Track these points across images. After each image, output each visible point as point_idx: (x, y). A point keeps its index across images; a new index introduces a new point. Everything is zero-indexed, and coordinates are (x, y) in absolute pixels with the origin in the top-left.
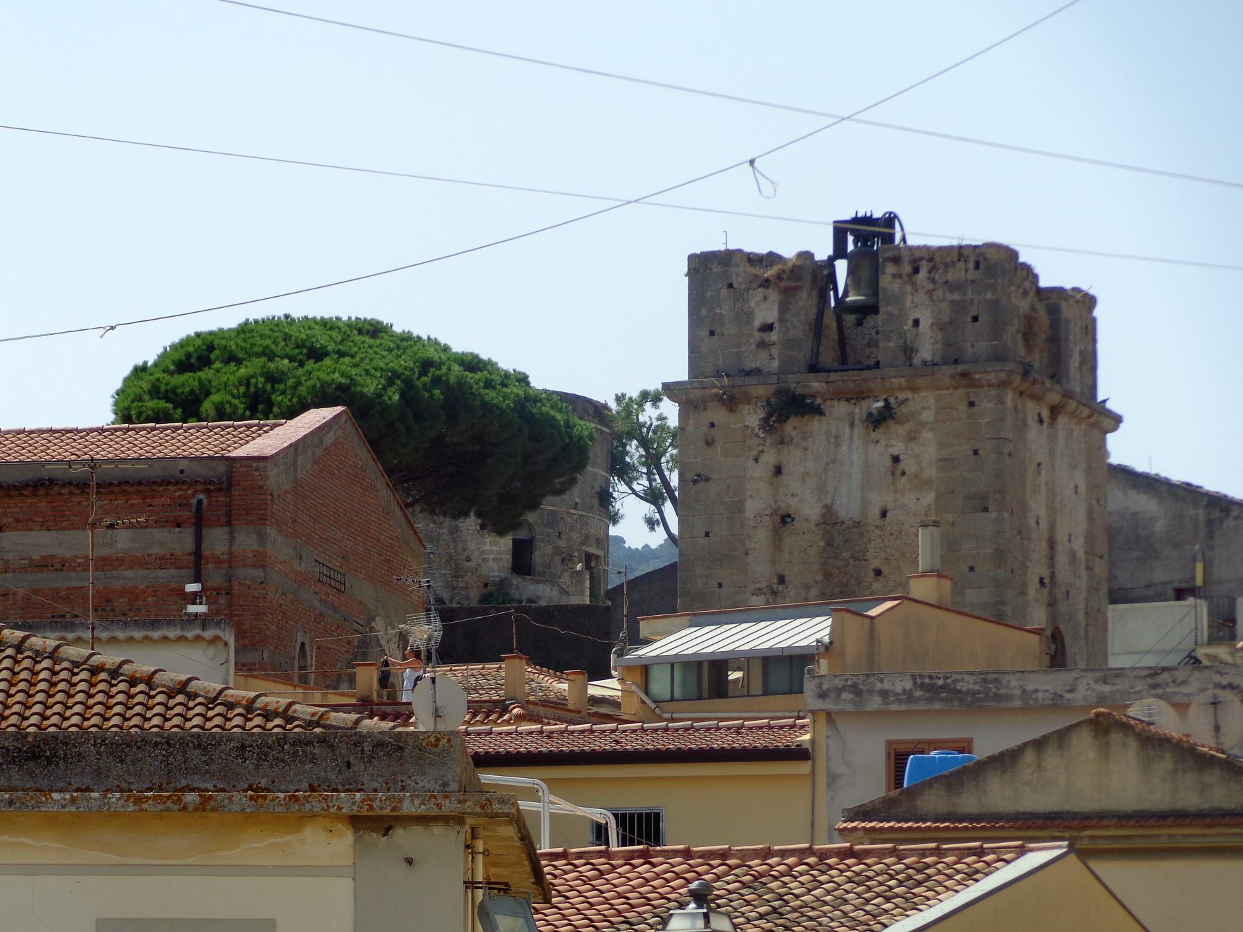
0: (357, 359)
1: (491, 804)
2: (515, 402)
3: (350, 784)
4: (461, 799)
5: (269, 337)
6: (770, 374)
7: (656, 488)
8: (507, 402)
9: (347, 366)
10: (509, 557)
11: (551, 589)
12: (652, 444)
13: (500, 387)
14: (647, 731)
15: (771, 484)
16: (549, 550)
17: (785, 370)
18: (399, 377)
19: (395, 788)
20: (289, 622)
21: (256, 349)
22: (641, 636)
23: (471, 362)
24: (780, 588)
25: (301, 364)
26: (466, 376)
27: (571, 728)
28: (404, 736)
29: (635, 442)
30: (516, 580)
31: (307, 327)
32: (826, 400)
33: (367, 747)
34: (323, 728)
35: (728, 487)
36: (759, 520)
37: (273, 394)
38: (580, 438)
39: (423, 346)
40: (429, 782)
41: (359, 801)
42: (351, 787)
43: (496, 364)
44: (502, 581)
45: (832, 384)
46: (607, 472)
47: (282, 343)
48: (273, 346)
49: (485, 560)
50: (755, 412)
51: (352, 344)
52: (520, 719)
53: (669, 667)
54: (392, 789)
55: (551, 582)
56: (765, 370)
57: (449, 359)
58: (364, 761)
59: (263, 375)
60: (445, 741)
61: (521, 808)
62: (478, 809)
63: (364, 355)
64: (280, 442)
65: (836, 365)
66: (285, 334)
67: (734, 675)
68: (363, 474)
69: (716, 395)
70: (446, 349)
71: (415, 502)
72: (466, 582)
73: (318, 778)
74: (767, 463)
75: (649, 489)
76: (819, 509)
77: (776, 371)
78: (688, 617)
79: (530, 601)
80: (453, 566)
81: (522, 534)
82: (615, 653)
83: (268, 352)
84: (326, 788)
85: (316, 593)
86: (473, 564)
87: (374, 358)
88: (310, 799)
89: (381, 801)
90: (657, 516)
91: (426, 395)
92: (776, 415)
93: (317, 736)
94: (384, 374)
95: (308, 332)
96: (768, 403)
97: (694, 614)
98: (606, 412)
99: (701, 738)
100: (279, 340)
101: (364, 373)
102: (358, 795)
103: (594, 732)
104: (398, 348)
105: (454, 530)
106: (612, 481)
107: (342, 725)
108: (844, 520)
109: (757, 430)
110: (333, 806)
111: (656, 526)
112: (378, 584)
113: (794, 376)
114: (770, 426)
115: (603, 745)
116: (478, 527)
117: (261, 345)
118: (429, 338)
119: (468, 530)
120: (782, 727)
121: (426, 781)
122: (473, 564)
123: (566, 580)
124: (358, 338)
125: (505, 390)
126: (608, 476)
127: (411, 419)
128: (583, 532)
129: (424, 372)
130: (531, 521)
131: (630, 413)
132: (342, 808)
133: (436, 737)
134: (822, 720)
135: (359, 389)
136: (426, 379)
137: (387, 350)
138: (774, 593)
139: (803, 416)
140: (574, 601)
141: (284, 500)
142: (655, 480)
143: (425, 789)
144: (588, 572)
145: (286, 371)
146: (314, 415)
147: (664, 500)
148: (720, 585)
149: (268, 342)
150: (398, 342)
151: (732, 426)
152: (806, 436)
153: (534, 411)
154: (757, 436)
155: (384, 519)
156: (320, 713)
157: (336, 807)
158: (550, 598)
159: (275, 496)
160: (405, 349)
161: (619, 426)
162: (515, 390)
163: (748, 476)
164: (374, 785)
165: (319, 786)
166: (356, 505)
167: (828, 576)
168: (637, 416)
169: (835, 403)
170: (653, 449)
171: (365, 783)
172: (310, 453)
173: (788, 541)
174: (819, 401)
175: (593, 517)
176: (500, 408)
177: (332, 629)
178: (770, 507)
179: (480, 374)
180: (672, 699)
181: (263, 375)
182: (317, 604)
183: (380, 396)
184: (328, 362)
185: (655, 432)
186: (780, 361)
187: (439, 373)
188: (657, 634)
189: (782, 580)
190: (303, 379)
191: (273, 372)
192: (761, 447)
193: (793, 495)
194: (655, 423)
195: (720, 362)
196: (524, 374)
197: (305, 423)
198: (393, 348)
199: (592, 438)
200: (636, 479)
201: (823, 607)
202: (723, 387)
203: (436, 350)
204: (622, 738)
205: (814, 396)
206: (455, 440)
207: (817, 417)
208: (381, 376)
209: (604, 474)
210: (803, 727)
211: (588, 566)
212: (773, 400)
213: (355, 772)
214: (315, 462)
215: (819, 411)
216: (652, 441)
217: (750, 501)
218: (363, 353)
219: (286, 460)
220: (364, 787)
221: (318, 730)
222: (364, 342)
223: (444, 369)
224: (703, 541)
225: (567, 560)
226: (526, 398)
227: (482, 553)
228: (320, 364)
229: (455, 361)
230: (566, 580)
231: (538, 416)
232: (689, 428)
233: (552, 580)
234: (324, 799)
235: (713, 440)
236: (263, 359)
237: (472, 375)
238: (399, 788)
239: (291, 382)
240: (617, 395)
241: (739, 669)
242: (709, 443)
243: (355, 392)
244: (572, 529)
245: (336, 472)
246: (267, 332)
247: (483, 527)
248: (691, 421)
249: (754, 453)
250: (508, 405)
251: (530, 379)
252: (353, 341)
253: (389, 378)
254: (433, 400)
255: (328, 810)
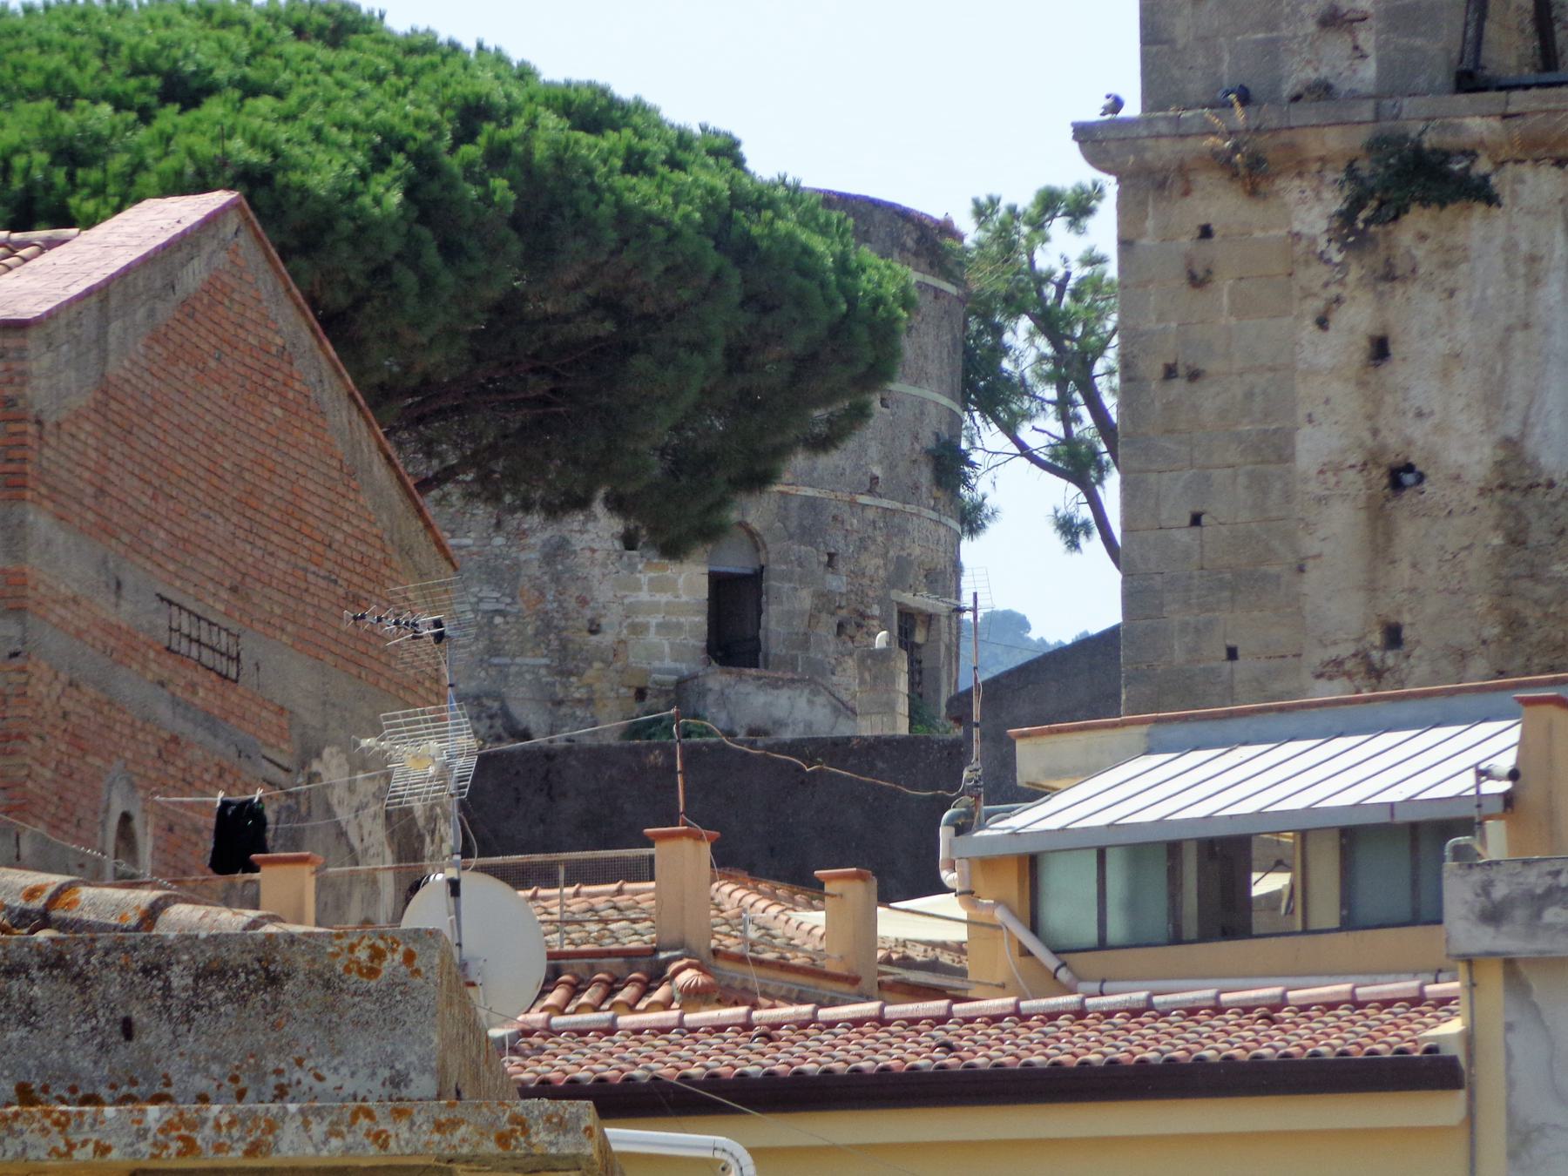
0: (292, 101)
1: (526, 1132)
2: (707, 209)
3: (133, 1082)
4: (443, 1118)
5: (63, 48)
6: (1355, 97)
7: (1082, 441)
8: (685, 208)
9: (265, 119)
10: (700, 620)
11: (811, 702)
12: (1070, 325)
13: (663, 170)
14: (1028, 1017)
15: (1362, 384)
16: (805, 600)
17: (1393, 86)
18: (400, 146)
19: (259, 1093)
20: (90, 759)
21: (29, 80)
22: (1021, 781)
23: (588, 106)
24: (1391, 658)
25: (146, 116)
26: (577, 142)
27: (825, 1013)
28: (283, 945)
29: (1025, 323)
30: (717, 679)
31: (159, 21)
32: (1503, 163)
33: (179, 979)
34: (59, 929)
35: (1249, 395)
36: (1332, 480)
37: (73, 192)
38: (878, 301)
39: (466, 66)
40: (353, 1074)
41: (154, 1127)
42: (134, 1091)
43: (656, 110)
44: (682, 684)
45: (1519, 121)
46: (953, 398)
47: (96, 63)
48: (72, 72)
49: (638, 629)
50: (1318, 197)
51: (278, 62)
52: (695, 997)
53: (1094, 853)
54: (250, 1094)
55: (811, 681)
56: (1343, 87)
57: (531, 98)
58: (170, 1019)
59: (44, 145)
60: (398, 957)
61: (615, 1147)
62: (490, 1147)
63: (309, 91)
64: (61, 284)
65: (1529, 75)
66: (104, 39)
67: (1266, 884)
68: (286, 368)
69: (1215, 154)
70: (525, 74)
71: (447, 475)
72: (590, 686)
73: (42, 1067)
74: (1352, 330)
75: (1063, 442)
76: (1487, 451)
77: (1371, 89)
78: (1144, 729)
79: (754, 732)
80: (555, 644)
81: (735, 561)
82: (949, 823)
83: (58, 85)
84: (67, 1095)
85: (162, 684)
86: (606, 639)
87: (337, 99)
88: (17, 1126)
89: (218, 1126)
90: (1086, 513)
91: (473, 192)
92: (1373, 204)
93: (38, 950)
94: (362, 138)
95: (163, 33)
96: (1351, 171)
97: (1158, 721)
98: (948, 242)
99: (1171, 1035)
100: (86, 55)
101: (309, 137)
102: (153, 1112)
103: (889, 1023)
104: (399, 71)
105: (557, 551)
106: (968, 422)
107: (113, 921)
108: (1556, 477)
109: (1322, 244)
110: (85, 1143)
111: (1082, 540)
112: (329, 658)
113: (1417, 100)
114: (1354, 231)
115: (916, 1054)
116: (618, 545)
117: (40, 69)
118: (480, 47)
119: (593, 551)
120: (1387, 1004)
121: (344, 1070)
122: (606, 639)
123: (848, 679)
124: (293, 48)
125: (678, 176)
126: (957, 409)
127: (432, 256)
128: (891, 553)
129: (466, 134)
130: (756, 526)
131: (1010, 247)
132: (108, 1149)
133: (372, 947)
134: (1493, 981)
135: (295, 177)
136: (468, 151)
137: (371, 78)
138: (1376, 674)
139: (1443, 205)
140: (868, 727)
141: (73, 436)
142: (1078, 419)
143: (343, 1093)
144: (904, 654)
145: (106, 132)
146: (151, 215)
147: (1102, 470)
148: (1232, 654)
149: (56, 60)
150: (399, 57)
151: (1258, 234)
152: (1450, 259)
153: (756, 230)
154: (1322, 258)
155: (341, 489)
156: (50, 890)
157: (91, 1147)
158: (809, 725)
159: (48, 426)
160: (418, 73)
161: (983, 280)
162: (705, 178)
163: (1301, 366)
164: (201, 1083)
165: (45, 1089)
166: (268, 451)
167: (1514, 624)
168: (1031, 254)
169: (1526, 170)
170: (1072, 339)
171: (174, 1079)
172: (141, 313)
173: (1409, 532)
174: (1483, 166)
175: (918, 515)
176: (666, 225)
177: (207, 777)
178: (1361, 445)
179: (612, 136)
180: (1102, 945)
181: (44, 145)
182: (163, 711)
183: (351, 195)
184: (214, 108)
185: (1077, 295)
186: (1380, 61)
187: (504, 134)
188: (1059, 773)
189: (1393, 636)
190: (151, 154)
191: (71, 139)
192: (1334, 290)
193: (1420, 414)
194: (1078, 272)
195: (1224, 67)
196: (729, 136)
197: (130, 236)
198: (385, 74)
199: (907, 302)
200: (1028, 416)
201: (1500, 696)
202: (1231, 133)
203: (497, 77)
204: (961, 1037)
205: (1471, 154)
206: (549, 307)
207: (1480, 209)
208: (354, 145)
209: (945, 401)
210: (1443, 1001)
211: (905, 637)
212: (1365, 167)
213: (147, 1049)
214: (157, 337)
215: (1482, 193)
216: (1068, 319)
217: (1307, 429)
218: (306, 85)
219: (77, 331)
220: (172, 1091)
221: (42, 935)
222: (309, 58)
223: (519, 125)
224: (1185, 536)
225: (851, 625)
226: (734, 198)
227: (631, 610)
228: (194, 114)
229: (549, 103)
230: (848, 679)
231: (764, 244)
232: (1144, 241)
233: (813, 678)
234: (56, 1123)
235: (1209, 272)
236: (46, 104)
237: (591, 139)
238: (270, 1091)
239: (118, 163)
240: (976, 202)
241: (1278, 866)
242: (1198, 280)
243: (287, 186)
244: (863, 546)
245: (212, 364)
246: (57, 36)
247: (629, 542)
248: (1150, 224)
249: (1318, 304)
250: (686, 217)
251: (745, 150)
252: (280, 56)
253: (375, 149)
254: (491, 204)
255: (68, 1154)
